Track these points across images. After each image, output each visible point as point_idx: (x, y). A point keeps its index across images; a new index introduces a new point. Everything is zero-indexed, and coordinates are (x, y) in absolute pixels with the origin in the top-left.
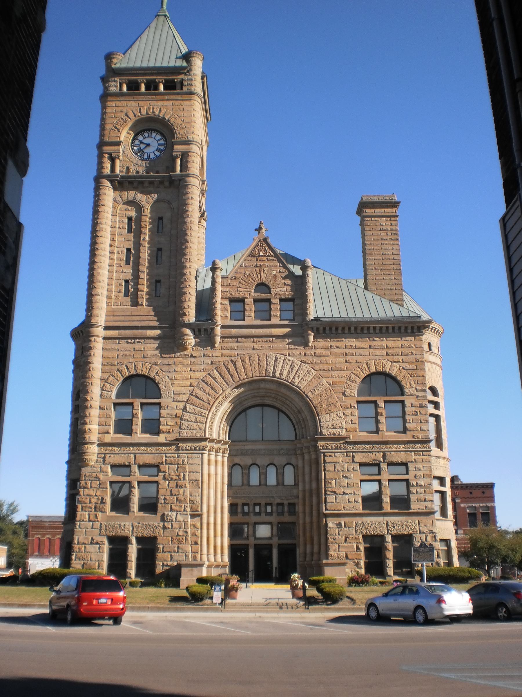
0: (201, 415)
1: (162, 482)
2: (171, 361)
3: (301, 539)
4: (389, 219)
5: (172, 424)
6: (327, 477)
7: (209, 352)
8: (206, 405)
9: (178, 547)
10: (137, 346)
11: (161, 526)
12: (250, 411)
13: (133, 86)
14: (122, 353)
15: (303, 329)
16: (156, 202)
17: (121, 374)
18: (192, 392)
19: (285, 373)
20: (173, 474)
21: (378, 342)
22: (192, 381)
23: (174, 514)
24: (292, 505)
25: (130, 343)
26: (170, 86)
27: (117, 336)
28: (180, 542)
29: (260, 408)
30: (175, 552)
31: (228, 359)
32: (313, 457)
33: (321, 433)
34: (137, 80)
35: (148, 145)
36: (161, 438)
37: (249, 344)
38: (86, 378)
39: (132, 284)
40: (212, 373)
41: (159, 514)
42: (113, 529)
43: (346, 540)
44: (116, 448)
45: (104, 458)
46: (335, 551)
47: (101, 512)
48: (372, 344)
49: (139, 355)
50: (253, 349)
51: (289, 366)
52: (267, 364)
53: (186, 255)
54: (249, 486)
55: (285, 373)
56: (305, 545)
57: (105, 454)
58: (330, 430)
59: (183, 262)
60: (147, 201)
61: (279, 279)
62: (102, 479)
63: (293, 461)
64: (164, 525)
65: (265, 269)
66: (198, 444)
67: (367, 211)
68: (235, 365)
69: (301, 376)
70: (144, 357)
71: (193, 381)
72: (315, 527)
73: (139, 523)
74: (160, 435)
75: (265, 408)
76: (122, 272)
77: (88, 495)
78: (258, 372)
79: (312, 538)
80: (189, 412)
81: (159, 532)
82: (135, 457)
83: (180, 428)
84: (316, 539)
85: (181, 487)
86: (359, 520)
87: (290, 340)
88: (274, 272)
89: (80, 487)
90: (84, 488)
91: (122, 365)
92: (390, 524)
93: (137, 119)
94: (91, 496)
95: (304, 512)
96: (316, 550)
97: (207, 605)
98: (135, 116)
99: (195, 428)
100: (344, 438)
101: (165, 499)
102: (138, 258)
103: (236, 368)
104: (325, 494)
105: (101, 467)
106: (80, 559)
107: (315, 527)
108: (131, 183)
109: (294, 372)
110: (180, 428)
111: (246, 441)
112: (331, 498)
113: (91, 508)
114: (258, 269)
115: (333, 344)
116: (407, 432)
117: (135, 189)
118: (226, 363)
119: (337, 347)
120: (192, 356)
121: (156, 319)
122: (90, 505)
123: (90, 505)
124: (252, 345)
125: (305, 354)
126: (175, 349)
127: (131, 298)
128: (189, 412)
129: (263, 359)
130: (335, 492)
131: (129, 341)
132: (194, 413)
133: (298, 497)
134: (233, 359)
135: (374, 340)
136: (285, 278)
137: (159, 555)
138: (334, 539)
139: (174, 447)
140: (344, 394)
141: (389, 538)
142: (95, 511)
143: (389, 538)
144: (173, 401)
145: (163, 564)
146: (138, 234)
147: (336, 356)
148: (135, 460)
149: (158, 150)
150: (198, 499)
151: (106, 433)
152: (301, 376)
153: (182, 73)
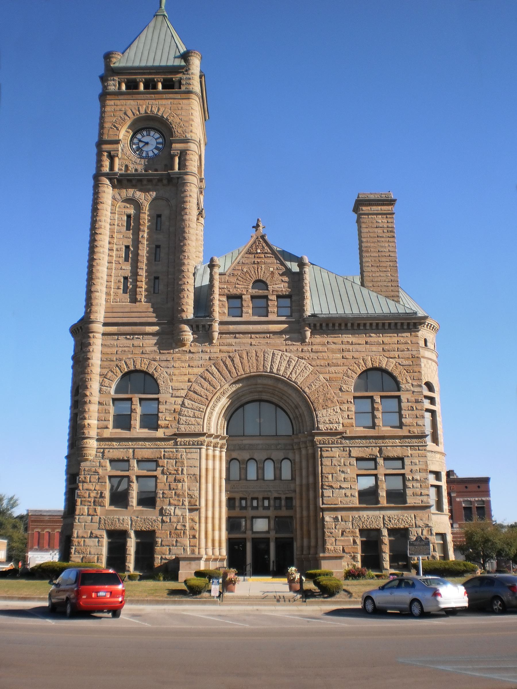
0: (199, 411)
1: (160, 476)
2: (169, 357)
3: (299, 532)
4: (385, 216)
5: (170, 419)
6: (324, 471)
7: (207, 348)
8: (204, 400)
9: (177, 541)
10: (136, 342)
11: (160, 520)
12: (247, 407)
13: (132, 85)
14: (120, 349)
15: (300, 325)
16: (154, 200)
17: (120, 369)
18: (190, 387)
19: (282, 369)
20: (171, 468)
21: (374, 338)
22: (191, 377)
23: (173, 508)
24: (289, 500)
25: (129, 339)
26: (169, 85)
27: (116, 332)
28: (178, 536)
29: (258, 403)
30: (173, 545)
31: (226, 354)
32: (310, 451)
33: (318, 428)
34: (135, 79)
35: (147, 143)
36: (160, 433)
37: (247, 340)
38: (86, 374)
39: (131, 280)
40: (209, 369)
41: (158, 508)
42: (112, 523)
43: (342, 534)
44: (114, 443)
45: (103, 453)
46: (332, 545)
47: (100, 506)
48: (369, 340)
49: (138, 351)
50: (251, 345)
51: (286, 362)
52: (264, 360)
53: (184, 252)
54: (247, 480)
55: (282, 369)
56: (302, 538)
57: (104, 449)
58: (327, 425)
59: (182, 259)
60: (145, 199)
61: (277, 276)
62: (101, 473)
63: (291, 456)
64: (162, 519)
65: (263, 266)
66: (196, 439)
67: (364, 208)
68: (233, 361)
69: (298, 372)
70: (142, 353)
71: (191, 377)
72: (312, 521)
73: (138, 517)
74: (159, 430)
75: (262, 403)
76: (121, 269)
77: (87, 490)
78: (255, 368)
79: (309, 532)
80: (187, 408)
81: (157, 526)
82: (134, 452)
83: (178, 423)
84: (313, 533)
85: (179, 481)
86: (356, 514)
87: (287, 337)
88: (271, 269)
89: (80, 482)
90: (84, 482)
91: (120, 360)
92: (386, 518)
93: (135, 117)
94: (90, 490)
95: (301, 507)
96: (313, 543)
97: (205, 598)
98: (134, 115)
99: (194, 423)
100: (341, 433)
101: (163, 493)
102: (136, 255)
103: (233, 364)
104: (322, 488)
105: (100, 462)
106: (79, 553)
107: (312, 521)
108: (129, 181)
109: (291, 368)
110: (178, 423)
111: (244, 436)
112: (328, 493)
113: (90, 502)
114: (256, 266)
115: (330, 340)
116: (404, 427)
117: (133, 187)
118: (224, 359)
119: (334, 343)
120: (190, 352)
121: (154, 315)
122: (89, 499)
123: (89, 499)
124: (249, 341)
125: (302, 350)
126: (174, 345)
127: (130, 295)
128: (187, 408)
129: (261, 355)
130: (331, 487)
131: (128, 337)
132: (192, 409)
133: (295, 491)
134: (231, 355)
135: (370, 336)
136: (282, 275)
137: (158, 549)
138: (331, 533)
139: (172, 442)
140: (340, 389)
141: (385, 532)
142: (94, 505)
143: (385, 532)
144: (172, 397)
145: (162, 557)
146: (137, 231)
147: (333, 351)
148: (133, 455)
149: (157, 148)
150: (197, 494)
151: (105, 428)
152: (298, 372)
153: (181, 72)
